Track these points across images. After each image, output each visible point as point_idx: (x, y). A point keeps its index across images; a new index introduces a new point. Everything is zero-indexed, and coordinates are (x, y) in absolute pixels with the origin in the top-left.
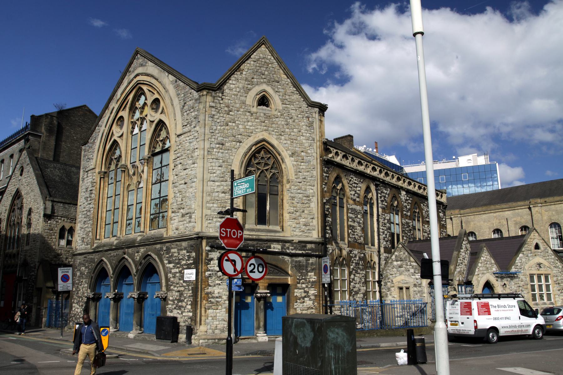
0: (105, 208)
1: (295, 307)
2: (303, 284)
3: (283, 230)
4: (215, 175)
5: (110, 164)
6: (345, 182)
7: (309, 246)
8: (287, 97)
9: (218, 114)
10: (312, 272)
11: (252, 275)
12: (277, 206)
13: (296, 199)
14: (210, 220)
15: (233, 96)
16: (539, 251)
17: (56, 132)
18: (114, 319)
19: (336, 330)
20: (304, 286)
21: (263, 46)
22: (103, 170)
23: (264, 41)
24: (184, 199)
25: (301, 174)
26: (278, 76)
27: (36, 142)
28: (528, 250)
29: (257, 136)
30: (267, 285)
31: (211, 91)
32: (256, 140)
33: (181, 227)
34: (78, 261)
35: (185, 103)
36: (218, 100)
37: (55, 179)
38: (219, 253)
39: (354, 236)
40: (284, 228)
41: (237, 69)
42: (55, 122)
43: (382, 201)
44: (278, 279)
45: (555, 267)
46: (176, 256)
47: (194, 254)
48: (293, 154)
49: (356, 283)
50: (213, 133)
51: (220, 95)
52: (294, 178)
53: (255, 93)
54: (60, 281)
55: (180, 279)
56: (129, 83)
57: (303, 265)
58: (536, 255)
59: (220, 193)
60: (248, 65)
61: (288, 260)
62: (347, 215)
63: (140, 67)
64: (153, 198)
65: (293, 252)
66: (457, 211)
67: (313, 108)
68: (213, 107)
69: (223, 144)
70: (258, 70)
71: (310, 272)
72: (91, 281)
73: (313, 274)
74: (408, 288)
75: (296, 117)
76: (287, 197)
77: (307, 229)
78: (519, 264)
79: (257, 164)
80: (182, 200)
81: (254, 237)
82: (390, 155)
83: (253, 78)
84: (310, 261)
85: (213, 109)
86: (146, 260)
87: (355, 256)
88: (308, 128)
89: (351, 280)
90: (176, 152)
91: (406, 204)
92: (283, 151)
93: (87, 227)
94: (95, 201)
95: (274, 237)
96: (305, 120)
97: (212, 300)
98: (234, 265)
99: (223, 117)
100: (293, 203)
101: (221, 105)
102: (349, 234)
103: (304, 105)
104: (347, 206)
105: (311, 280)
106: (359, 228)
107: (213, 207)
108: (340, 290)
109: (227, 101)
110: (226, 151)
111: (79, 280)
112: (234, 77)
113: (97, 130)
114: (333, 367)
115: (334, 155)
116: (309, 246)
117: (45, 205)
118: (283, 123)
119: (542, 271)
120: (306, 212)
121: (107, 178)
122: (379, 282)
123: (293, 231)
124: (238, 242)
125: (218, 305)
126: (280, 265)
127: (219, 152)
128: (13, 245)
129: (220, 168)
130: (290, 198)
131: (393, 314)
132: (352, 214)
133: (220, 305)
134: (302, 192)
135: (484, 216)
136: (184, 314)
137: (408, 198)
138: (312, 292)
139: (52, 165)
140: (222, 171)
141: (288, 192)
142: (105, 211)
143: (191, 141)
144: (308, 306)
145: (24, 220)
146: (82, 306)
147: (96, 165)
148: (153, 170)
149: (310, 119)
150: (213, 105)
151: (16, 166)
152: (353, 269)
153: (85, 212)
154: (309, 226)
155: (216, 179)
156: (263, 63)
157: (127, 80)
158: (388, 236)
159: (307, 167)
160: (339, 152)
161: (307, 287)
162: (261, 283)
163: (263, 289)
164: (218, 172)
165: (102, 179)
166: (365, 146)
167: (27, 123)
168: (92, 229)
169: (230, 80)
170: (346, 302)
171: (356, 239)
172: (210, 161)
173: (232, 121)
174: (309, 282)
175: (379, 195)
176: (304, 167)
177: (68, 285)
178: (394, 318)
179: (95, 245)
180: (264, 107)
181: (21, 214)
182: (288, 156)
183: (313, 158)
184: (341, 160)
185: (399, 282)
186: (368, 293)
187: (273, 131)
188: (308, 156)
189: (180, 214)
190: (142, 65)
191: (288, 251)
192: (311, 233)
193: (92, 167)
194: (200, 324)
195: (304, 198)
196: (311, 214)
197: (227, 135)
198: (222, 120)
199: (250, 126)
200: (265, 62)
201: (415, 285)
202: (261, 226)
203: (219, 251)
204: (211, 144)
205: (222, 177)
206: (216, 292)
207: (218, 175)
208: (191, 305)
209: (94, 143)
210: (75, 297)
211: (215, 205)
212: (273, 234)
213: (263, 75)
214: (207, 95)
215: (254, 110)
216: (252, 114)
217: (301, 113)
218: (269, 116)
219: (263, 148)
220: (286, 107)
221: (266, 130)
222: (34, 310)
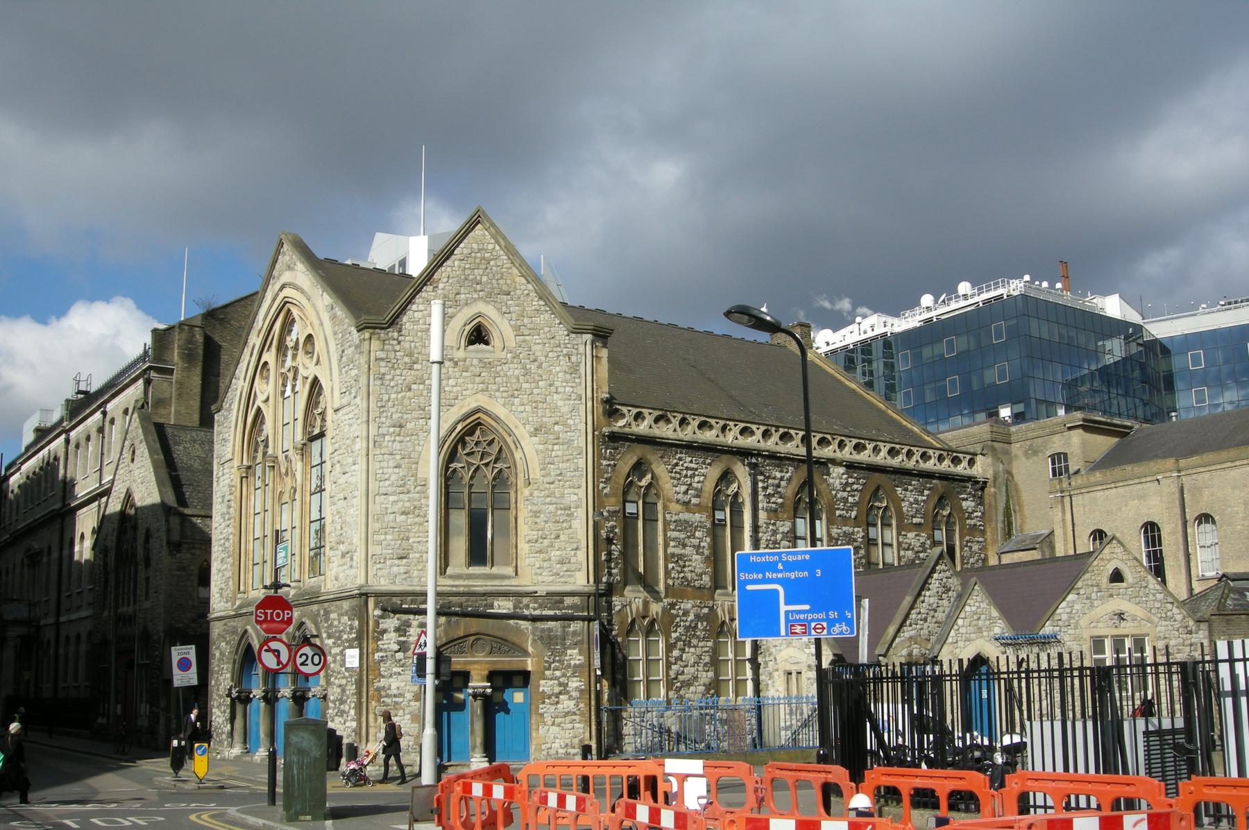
0: (252, 534)
1: (540, 711)
2: (557, 670)
3: (516, 574)
4: (387, 483)
5: (256, 451)
6: (661, 469)
7: (568, 601)
8: (526, 321)
9: (392, 372)
10: (574, 649)
11: (303, 669)
12: (508, 529)
13: (542, 516)
14: (380, 563)
15: (419, 334)
16: (1124, 585)
17: (201, 358)
18: (266, 735)
19: (301, 734)
20: (558, 673)
21: (479, 226)
22: (245, 462)
23: (479, 216)
24: (343, 526)
25: (552, 466)
26: (509, 282)
27: (165, 384)
28: (1092, 585)
29: (467, 404)
30: (486, 673)
31: (377, 331)
32: (464, 410)
33: (341, 576)
34: (217, 630)
35: (343, 351)
36: (392, 345)
37: (192, 466)
38: (398, 619)
39: (682, 575)
40: (519, 569)
41: (428, 280)
42: (198, 336)
43: (769, 496)
44: (507, 662)
45: (1166, 619)
46: (335, 626)
47: (356, 623)
48: (536, 430)
49: (687, 666)
50: (382, 407)
51: (396, 334)
52: (538, 476)
53: (462, 323)
54: (176, 670)
55: (341, 666)
56: (274, 300)
57: (556, 636)
58: (1111, 596)
59: (398, 515)
60: (449, 269)
61: (527, 629)
62: (665, 535)
63: (286, 270)
64: (312, 519)
65: (537, 612)
66: (1170, 463)
67: (579, 335)
68: (382, 359)
69: (401, 426)
70: (468, 275)
71: (571, 649)
72: (233, 668)
73: (576, 651)
75: (543, 358)
76: (523, 513)
77: (565, 569)
78: (1064, 617)
79: (468, 454)
80: (342, 528)
81: (462, 589)
82: (1105, 293)
83: (457, 294)
84: (572, 629)
85: (383, 364)
86: (301, 631)
87: (686, 613)
88: (568, 377)
89: (673, 660)
90: (333, 441)
91: (845, 494)
92: (516, 427)
93: (226, 569)
94: (235, 522)
95: (500, 588)
96: (564, 361)
97: (386, 700)
98: (278, 657)
99: (401, 375)
100: (536, 523)
101: (398, 353)
102: (667, 573)
104: (664, 517)
105: (572, 663)
106: (698, 557)
107: (385, 539)
108: (643, 680)
109: (407, 345)
110: (408, 439)
111: (218, 666)
112: (421, 297)
113: (233, 387)
114: (295, 772)
115: (632, 420)
116: (568, 601)
117: (169, 524)
118: (517, 372)
119: (1126, 628)
120: (562, 537)
121: (252, 478)
122: (754, 662)
123: (536, 574)
124: (285, 626)
125: (397, 709)
126: (510, 638)
127: (394, 441)
128: (129, 598)
129: (397, 470)
130: (530, 514)
131: (776, 723)
132: (679, 531)
133: (401, 708)
134: (554, 500)
135: (1233, 474)
136: (347, 724)
138: (575, 684)
139: (189, 436)
140: (401, 474)
141: (526, 503)
142: (252, 540)
143: (351, 421)
144: (566, 710)
145: (140, 552)
146: (225, 712)
147: (233, 454)
148: (312, 467)
149: (574, 358)
150: (381, 355)
151: (124, 443)
152: (678, 639)
153: (222, 541)
154: (569, 563)
155: (390, 490)
156: (478, 261)
157: (270, 295)
159: (567, 453)
161: (564, 675)
162: (475, 669)
163: (478, 681)
164: (393, 478)
165: (244, 479)
166: (1027, 278)
167: (145, 344)
168: (233, 574)
169: (414, 303)
170: (660, 703)
171: (687, 580)
172: (379, 459)
173: (418, 381)
174: (569, 666)
175: (760, 485)
176: (559, 453)
177: (191, 676)
178: (777, 730)
179: (238, 603)
180: (483, 346)
181: (135, 539)
182: (527, 435)
183: (578, 434)
184: (650, 427)
185: (786, 660)
186: (722, 683)
187: (499, 390)
188: (567, 432)
189: (339, 553)
190: (289, 268)
191: (526, 612)
192: (573, 576)
193: (229, 456)
194: (367, 741)
195: (559, 512)
196: (573, 540)
197: (409, 407)
198: (399, 382)
199: (453, 386)
200: (483, 258)
202: (477, 568)
203: (397, 616)
204: (379, 427)
205: (401, 486)
206: (393, 687)
207: (393, 484)
208: (355, 708)
209: (230, 410)
210: (215, 696)
211: (389, 537)
212: (496, 582)
213: (478, 284)
214: (370, 338)
215: (460, 354)
216: (456, 364)
217: (555, 349)
218: (490, 363)
220: (525, 341)
221: (482, 391)
222: (162, 720)
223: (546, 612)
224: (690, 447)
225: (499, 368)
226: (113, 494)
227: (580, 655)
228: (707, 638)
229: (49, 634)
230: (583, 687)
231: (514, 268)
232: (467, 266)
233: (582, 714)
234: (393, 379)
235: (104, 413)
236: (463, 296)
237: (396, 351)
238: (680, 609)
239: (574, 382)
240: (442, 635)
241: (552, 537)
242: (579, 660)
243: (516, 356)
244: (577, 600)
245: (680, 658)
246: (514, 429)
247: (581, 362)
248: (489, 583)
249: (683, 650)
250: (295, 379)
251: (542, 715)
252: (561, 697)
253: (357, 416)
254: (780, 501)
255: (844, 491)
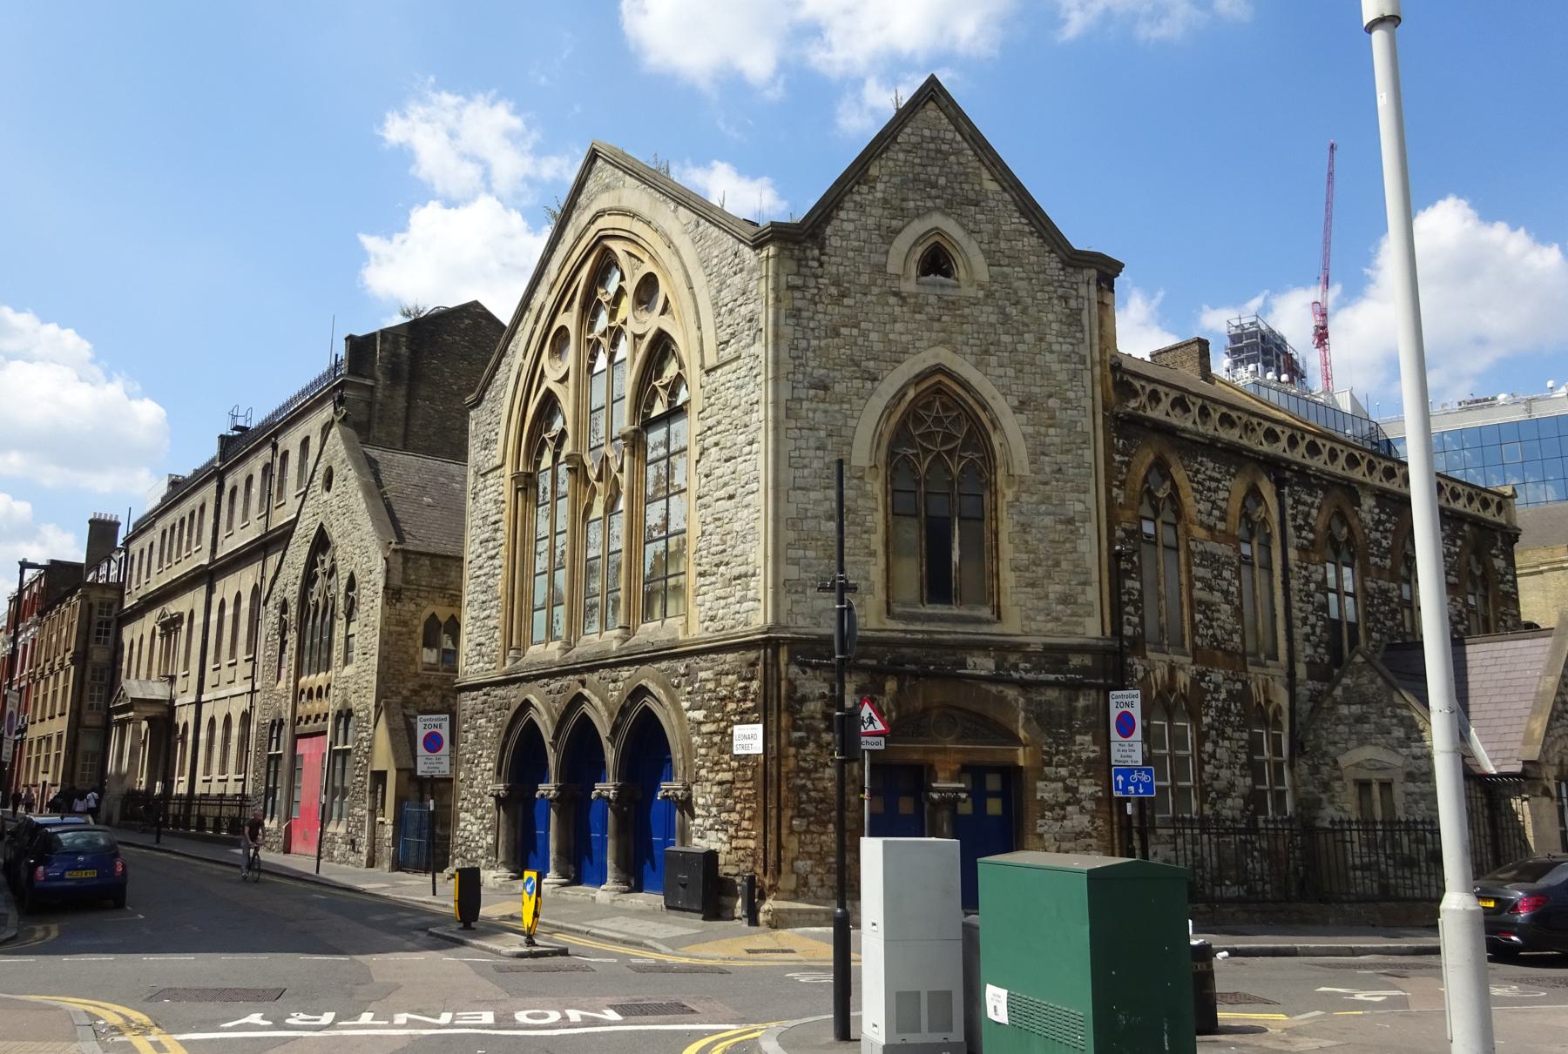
1: (1039, 830)
2: (1062, 766)
3: (999, 617)
4: (806, 472)
5: (540, 454)
6: (1179, 474)
7: (1075, 661)
8: (1003, 245)
12: (983, 548)
13: (1034, 531)
14: (796, 592)
15: (851, 254)
20: (1063, 772)
25: (1047, 459)
43: (1299, 528)
48: (1022, 403)
50: (798, 357)
52: (1027, 473)
56: (579, 238)
62: (1189, 571)
65: (1031, 676)
69: (826, 388)
73: (1088, 738)
74: (1386, 786)
75: (1029, 301)
85: (798, 294)
87: (1217, 688)
88: (1065, 328)
89: (1205, 757)
96: (1058, 306)
101: (820, 280)
102: (1194, 627)
103: (1053, 264)
105: (1084, 756)
109: (834, 269)
116: (1075, 661)
120: (1064, 565)
129: (820, 453)
130: (1017, 528)
134: (1051, 508)
137: (1383, 517)
141: (1012, 511)
144: (1078, 830)
149: (1073, 303)
152: (1211, 727)
154: (1075, 603)
157: (572, 232)
158: (1318, 631)
160: (1161, 389)
161: (1072, 775)
163: (946, 780)
169: (842, 209)
172: (794, 435)
174: (1079, 760)
175: (1290, 511)
180: (940, 278)
182: (1009, 411)
188: (1066, 409)
191: (1015, 675)
193: (498, 461)
198: (823, 323)
200: (939, 151)
201: (1410, 777)
211: (811, 554)
212: (970, 628)
215: (909, 286)
217: (1046, 288)
218: (953, 303)
219: (938, 390)
223: (1043, 677)
224: (1211, 447)
225: (967, 311)
226: (300, 530)
227: (1095, 744)
228: (1242, 726)
229: (185, 716)
230: (1100, 794)
231: (983, 169)
232: (917, 161)
233: (1100, 837)
234: (812, 319)
235: (275, 447)
236: (911, 204)
237: (816, 277)
238: (1210, 681)
239: (1074, 337)
240: (892, 707)
241: (1050, 563)
242: (1094, 752)
243: (990, 295)
244: (1088, 660)
245: (1213, 755)
246: (990, 401)
247: (1081, 310)
248: (959, 630)
249: (1215, 743)
250: (614, 345)
251: (1041, 836)
252: (1069, 808)
253: (755, 372)
254: (1311, 536)
255: (1377, 530)
